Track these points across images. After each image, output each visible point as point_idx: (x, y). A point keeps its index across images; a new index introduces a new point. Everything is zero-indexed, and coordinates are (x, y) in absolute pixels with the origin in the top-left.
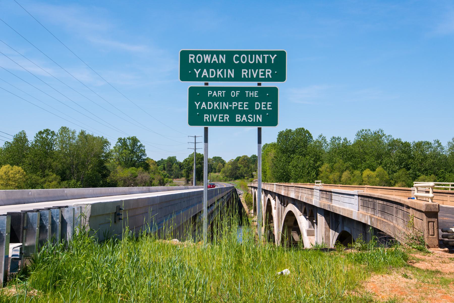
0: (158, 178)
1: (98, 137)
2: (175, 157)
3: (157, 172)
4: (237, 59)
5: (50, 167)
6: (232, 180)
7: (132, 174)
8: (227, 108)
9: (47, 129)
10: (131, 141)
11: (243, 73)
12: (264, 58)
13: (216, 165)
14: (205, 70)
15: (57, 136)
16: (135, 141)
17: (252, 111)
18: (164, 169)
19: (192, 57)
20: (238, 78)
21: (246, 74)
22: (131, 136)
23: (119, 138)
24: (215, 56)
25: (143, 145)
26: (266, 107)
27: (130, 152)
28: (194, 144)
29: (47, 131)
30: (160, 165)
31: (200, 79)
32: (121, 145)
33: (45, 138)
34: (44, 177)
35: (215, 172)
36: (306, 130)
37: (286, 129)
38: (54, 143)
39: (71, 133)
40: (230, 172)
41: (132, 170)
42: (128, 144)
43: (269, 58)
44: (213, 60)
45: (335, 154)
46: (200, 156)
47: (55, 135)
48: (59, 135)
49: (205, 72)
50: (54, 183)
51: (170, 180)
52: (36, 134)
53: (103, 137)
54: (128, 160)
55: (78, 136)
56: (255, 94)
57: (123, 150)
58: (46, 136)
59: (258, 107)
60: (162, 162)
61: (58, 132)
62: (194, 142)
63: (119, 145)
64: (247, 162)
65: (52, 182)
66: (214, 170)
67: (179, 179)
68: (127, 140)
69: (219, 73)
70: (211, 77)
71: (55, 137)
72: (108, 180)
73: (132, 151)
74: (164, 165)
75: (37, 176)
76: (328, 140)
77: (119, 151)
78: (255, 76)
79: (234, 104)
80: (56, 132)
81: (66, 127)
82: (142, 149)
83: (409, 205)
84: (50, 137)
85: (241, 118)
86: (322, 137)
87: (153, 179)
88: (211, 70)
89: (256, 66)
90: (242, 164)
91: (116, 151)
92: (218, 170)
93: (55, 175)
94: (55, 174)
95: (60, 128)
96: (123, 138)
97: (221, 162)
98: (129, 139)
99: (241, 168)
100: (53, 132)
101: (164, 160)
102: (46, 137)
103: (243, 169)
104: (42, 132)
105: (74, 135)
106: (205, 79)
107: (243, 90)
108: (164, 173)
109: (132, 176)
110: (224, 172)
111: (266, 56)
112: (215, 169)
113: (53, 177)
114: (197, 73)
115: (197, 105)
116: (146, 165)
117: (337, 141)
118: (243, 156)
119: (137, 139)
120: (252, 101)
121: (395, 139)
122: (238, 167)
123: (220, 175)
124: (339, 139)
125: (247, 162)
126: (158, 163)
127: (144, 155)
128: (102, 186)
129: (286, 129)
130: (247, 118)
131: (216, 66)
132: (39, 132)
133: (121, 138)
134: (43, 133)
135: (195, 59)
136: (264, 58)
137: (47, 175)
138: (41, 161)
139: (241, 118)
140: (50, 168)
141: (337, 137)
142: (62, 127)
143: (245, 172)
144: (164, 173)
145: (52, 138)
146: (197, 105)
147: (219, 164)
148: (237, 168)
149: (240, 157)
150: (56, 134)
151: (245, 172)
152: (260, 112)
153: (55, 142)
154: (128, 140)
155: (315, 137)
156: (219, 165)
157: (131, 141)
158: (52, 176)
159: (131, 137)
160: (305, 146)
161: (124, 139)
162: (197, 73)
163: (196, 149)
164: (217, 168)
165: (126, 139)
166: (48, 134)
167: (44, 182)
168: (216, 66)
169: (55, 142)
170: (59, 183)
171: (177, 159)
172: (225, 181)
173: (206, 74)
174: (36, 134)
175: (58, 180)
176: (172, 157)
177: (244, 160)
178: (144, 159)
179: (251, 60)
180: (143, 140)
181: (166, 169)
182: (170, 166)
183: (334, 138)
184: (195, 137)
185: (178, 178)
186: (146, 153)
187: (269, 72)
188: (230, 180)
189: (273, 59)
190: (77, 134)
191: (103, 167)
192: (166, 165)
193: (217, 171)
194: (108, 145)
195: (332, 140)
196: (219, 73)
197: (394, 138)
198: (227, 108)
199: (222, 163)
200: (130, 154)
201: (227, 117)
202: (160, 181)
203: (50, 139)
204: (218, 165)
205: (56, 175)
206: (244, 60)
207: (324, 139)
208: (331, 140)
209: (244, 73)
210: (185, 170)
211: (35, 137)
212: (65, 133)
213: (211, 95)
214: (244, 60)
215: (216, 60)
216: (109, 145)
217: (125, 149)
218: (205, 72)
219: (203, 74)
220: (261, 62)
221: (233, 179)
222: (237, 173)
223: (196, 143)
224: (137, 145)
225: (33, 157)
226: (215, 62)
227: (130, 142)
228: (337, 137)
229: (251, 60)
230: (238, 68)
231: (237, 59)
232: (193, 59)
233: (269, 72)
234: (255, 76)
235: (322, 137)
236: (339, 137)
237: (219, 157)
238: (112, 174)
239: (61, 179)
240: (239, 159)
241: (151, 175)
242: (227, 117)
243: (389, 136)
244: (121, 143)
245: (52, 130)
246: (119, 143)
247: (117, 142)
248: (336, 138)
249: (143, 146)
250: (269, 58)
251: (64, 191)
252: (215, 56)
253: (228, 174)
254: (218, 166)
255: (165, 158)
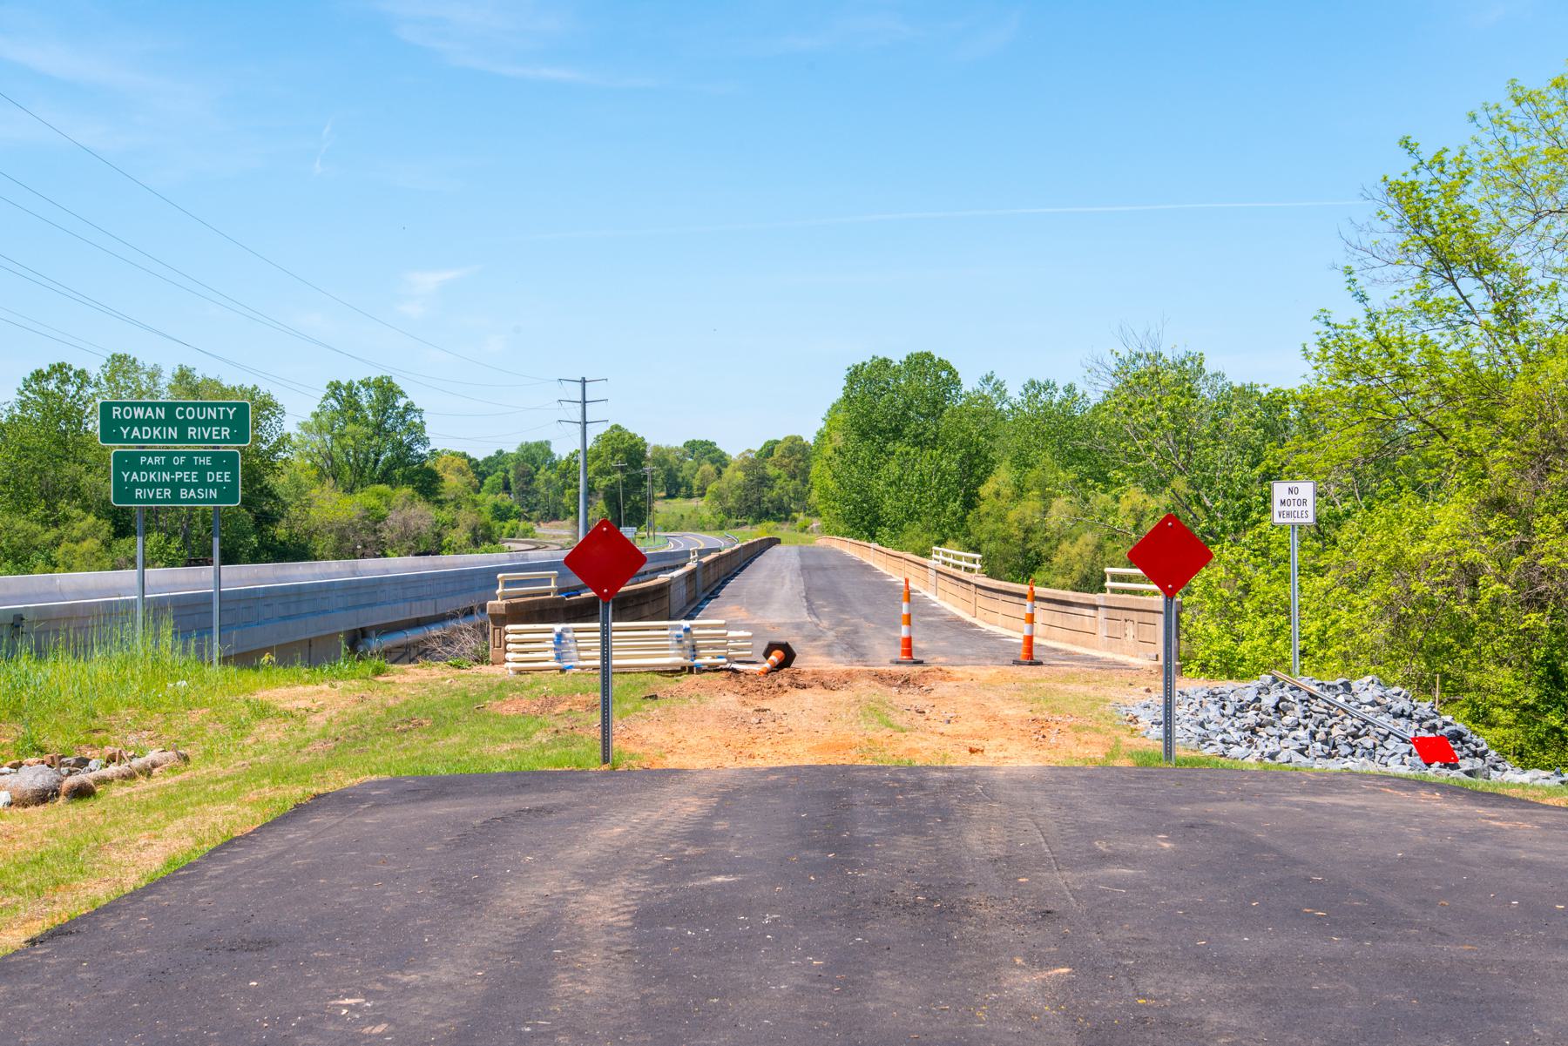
0: (469, 522)
1: (241, 386)
2: (548, 443)
3: (468, 500)
4: (181, 413)
5: (75, 493)
6: (746, 523)
7: (367, 509)
8: (168, 480)
9: (59, 365)
10: (372, 393)
11: (190, 433)
12: (218, 412)
13: (692, 472)
14: (136, 429)
15: (96, 385)
16: (386, 391)
17: (203, 483)
18: (507, 487)
19: (117, 410)
20: (183, 438)
21: (193, 433)
22: (374, 375)
23: (332, 383)
24: (149, 409)
25: (417, 407)
26: (223, 478)
27: (370, 431)
28: (579, 407)
29: (60, 368)
30: (491, 471)
31: (129, 440)
32: (339, 408)
33: (53, 394)
34: (56, 524)
35: (689, 496)
36: (940, 360)
37: (874, 357)
38: (89, 410)
39: (144, 377)
40: (740, 496)
41: (367, 498)
42: (364, 403)
43: (225, 412)
44: (148, 414)
45: (1036, 439)
46: (623, 443)
47: (89, 383)
48: (103, 381)
49: (136, 431)
50: (91, 544)
51: (523, 525)
52: (25, 380)
53: (255, 387)
54: (367, 460)
55: (170, 386)
56: (207, 461)
57: (346, 423)
58: (58, 388)
59: (211, 478)
60: (499, 463)
61: (100, 372)
62: (580, 398)
63: (332, 406)
64: (800, 460)
65: (84, 540)
66: (683, 489)
67: (557, 523)
68: (358, 388)
69: (156, 432)
70: (144, 437)
71: (91, 391)
72: (281, 532)
73: (379, 428)
74: (507, 472)
75: (30, 524)
76: (1015, 393)
77: (332, 427)
78: (206, 436)
79: (178, 475)
80: (94, 371)
81: (126, 357)
82: (414, 420)
83: (1097, 603)
84: (72, 389)
85: (188, 493)
86: (994, 381)
87: (444, 525)
88: (144, 428)
89: (208, 423)
90: (782, 466)
91: (320, 428)
92: (698, 490)
93: (91, 519)
94: (92, 515)
95: (108, 361)
96: (344, 383)
97: (710, 459)
98: (366, 384)
99: (779, 482)
100: (83, 372)
101: (507, 454)
102: (56, 390)
103: (783, 487)
104: (43, 375)
105: (155, 385)
106: (136, 440)
107: (190, 456)
108: (503, 500)
109: (364, 518)
110: (719, 496)
111: (222, 409)
112: (689, 487)
113: (84, 525)
114: (125, 432)
115: (126, 476)
116: (427, 483)
117: (1043, 397)
118: (786, 439)
119: (394, 385)
120: (202, 470)
121: (1237, 385)
122: (769, 480)
123: (701, 506)
124: (1049, 386)
125: (800, 460)
126: (480, 471)
127: (425, 442)
128: (255, 558)
129: (874, 357)
130: (197, 494)
131: (151, 423)
132: (32, 374)
133: (338, 382)
134: (47, 377)
135: (121, 414)
136: (218, 412)
137: (67, 518)
138: (43, 471)
139: (188, 493)
140: (75, 495)
141: (1043, 382)
142: (113, 356)
143: (792, 495)
144: (503, 500)
145: (78, 393)
146: (126, 476)
147: (702, 468)
148: (764, 481)
149: (777, 442)
150: (93, 379)
151: (792, 495)
152: (214, 485)
153: (91, 406)
154: (363, 390)
155: (970, 383)
156: (704, 472)
157: (372, 393)
158: (81, 521)
159: (372, 380)
160: (936, 408)
161: (351, 385)
162: (125, 432)
163: (585, 423)
164: (696, 483)
165: (356, 384)
166: (65, 380)
167: (56, 543)
168: (151, 423)
169: (91, 406)
170: (107, 545)
171: (553, 450)
172: (721, 527)
173: (138, 434)
174: (25, 380)
175: (103, 534)
176: (536, 444)
177: (791, 451)
178: (420, 456)
179: (201, 415)
180: (414, 392)
181: (513, 487)
182: (528, 478)
183: (1032, 384)
184: (584, 381)
185: (555, 517)
186: (426, 435)
187: (226, 431)
188: (737, 525)
189: (231, 413)
190: (166, 379)
191: (261, 491)
192: (511, 475)
193: (695, 492)
194: (274, 415)
195: (1026, 390)
196: (156, 432)
197: (1231, 383)
198: (168, 480)
199: (713, 462)
200: (370, 438)
201: (167, 493)
202: (474, 530)
203: (74, 397)
204: (699, 473)
205: (94, 518)
206: (190, 414)
207: (999, 388)
208: (1023, 391)
209: (192, 432)
210: (571, 490)
211: (19, 389)
212: (123, 376)
213: (145, 463)
214: (190, 414)
215: (152, 415)
216: (280, 416)
217: (354, 420)
218: (136, 431)
219: (134, 434)
220: (215, 416)
221: (750, 520)
222: (765, 499)
223: (584, 402)
224: (394, 407)
225: (13, 458)
226: (150, 417)
227: (370, 396)
228: (1043, 382)
229: (201, 415)
230: (183, 426)
231: (181, 413)
232: (118, 413)
233: (226, 431)
234: (206, 436)
235: (994, 381)
236: (1051, 383)
237: (706, 443)
238: (294, 512)
239: (112, 529)
240: (773, 449)
241: (445, 515)
242: (167, 493)
243: (1215, 375)
244: (337, 399)
245: (77, 367)
246: (332, 401)
247: (326, 398)
248: (1039, 384)
249: (416, 411)
250: (225, 412)
251: (52, 580)
252: (149, 409)
253: (731, 502)
254: (698, 475)
255: (511, 448)
